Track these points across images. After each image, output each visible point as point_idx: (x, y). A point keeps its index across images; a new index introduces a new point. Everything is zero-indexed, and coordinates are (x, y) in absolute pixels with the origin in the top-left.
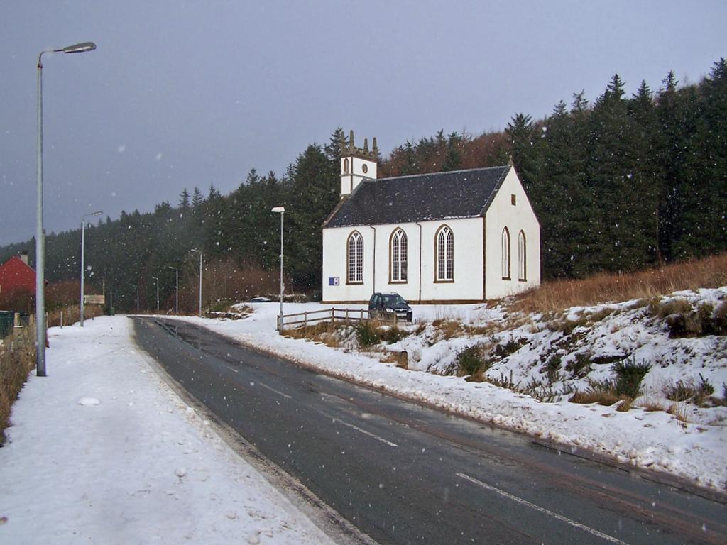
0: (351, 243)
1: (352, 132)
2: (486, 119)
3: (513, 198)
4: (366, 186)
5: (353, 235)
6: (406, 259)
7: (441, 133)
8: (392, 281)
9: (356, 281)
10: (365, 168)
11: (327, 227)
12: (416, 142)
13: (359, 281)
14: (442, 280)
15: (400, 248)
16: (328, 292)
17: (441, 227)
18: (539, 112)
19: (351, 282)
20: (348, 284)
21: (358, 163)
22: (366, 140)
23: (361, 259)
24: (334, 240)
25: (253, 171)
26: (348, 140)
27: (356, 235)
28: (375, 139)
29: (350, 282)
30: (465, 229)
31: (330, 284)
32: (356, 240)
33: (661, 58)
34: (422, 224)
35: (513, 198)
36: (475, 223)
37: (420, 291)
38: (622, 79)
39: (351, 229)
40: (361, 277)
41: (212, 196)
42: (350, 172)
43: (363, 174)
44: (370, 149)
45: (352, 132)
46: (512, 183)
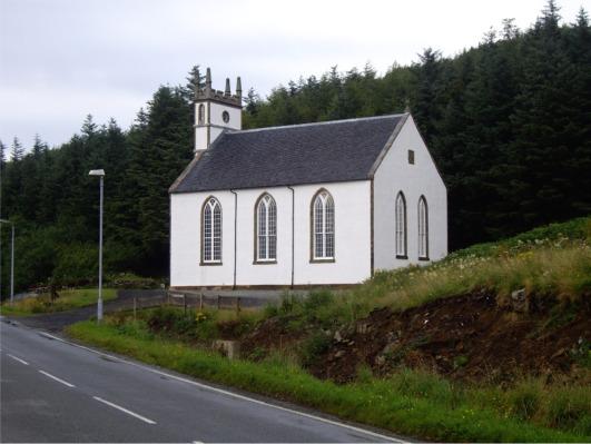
0: (206, 213)
1: (209, 70)
2: (385, 51)
3: (411, 154)
4: (227, 141)
6: (275, 232)
7: (334, 69)
8: (315, 258)
10: (226, 116)
11: (176, 192)
12: (343, 73)
15: (266, 222)
17: (207, 200)
18: (452, 45)
21: (217, 110)
22: (228, 81)
23: (218, 231)
24: (185, 211)
25: (90, 117)
26: (204, 81)
27: (213, 202)
30: (350, 199)
32: (212, 208)
34: (296, 189)
35: (411, 154)
36: (363, 188)
38: (557, 3)
39: (205, 196)
41: (37, 148)
42: (206, 122)
43: (223, 124)
44: (233, 92)
45: (209, 70)
46: (409, 135)
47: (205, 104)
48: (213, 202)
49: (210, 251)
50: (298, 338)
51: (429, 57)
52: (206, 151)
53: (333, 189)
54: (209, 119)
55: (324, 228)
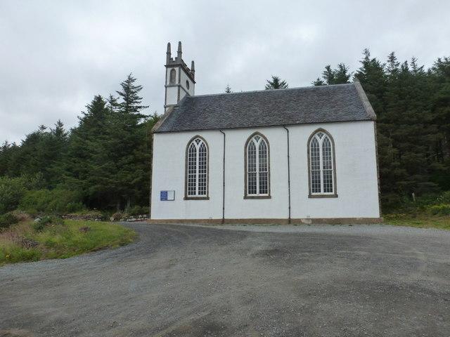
0: (190, 152)
5: (194, 142)
8: (333, 193)
9: (197, 195)
13: (201, 196)
14: (318, 194)
16: (159, 211)
19: (190, 196)
20: (186, 198)
22: (169, 45)
27: (198, 142)
28: (180, 43)
29: (189, 196)
31: (161, 200)
32: (198, 147)
33: (420, 46)
34: (290, 129)
37: (290, 208)
39: (190, 136)
40: (204, 189)
42: (177, 83)
45: (193, 62)
47: (177, 69)
48: (198, 142)
49: (196, 185)
50: (417, 331)
51: (276, 83)
52: (176, 106)
53: (332, 129)
54: (179, 80)
55: (197, 170)
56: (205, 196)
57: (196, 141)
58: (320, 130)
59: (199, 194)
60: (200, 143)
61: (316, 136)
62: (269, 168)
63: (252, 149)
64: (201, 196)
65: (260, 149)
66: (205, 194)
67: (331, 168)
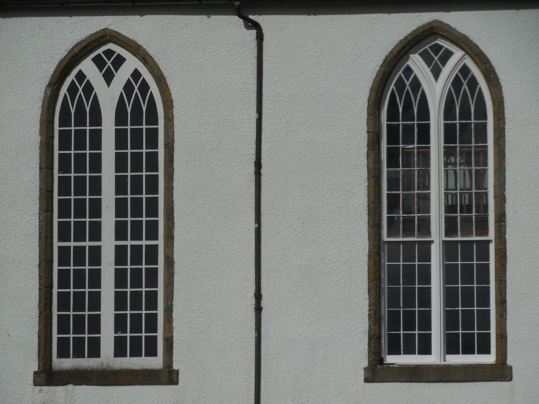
0: (67, 118)
5: (87, 66)
13: (130, 362)
14: (86, 363)
32: (108, 96)
34: (267, 21)
48: (109, 67)
55: (108, 219)
56: (155, 363)
57: (99, 62)
58: (105, 37)
59: (120, 351)
60: (123, 75)
61: (416, 62)
62: (501, 218)
63: (465, 114)
64: (130, 362)
65: (449, 112)
66: (152, 352)
67: (483, 229)
